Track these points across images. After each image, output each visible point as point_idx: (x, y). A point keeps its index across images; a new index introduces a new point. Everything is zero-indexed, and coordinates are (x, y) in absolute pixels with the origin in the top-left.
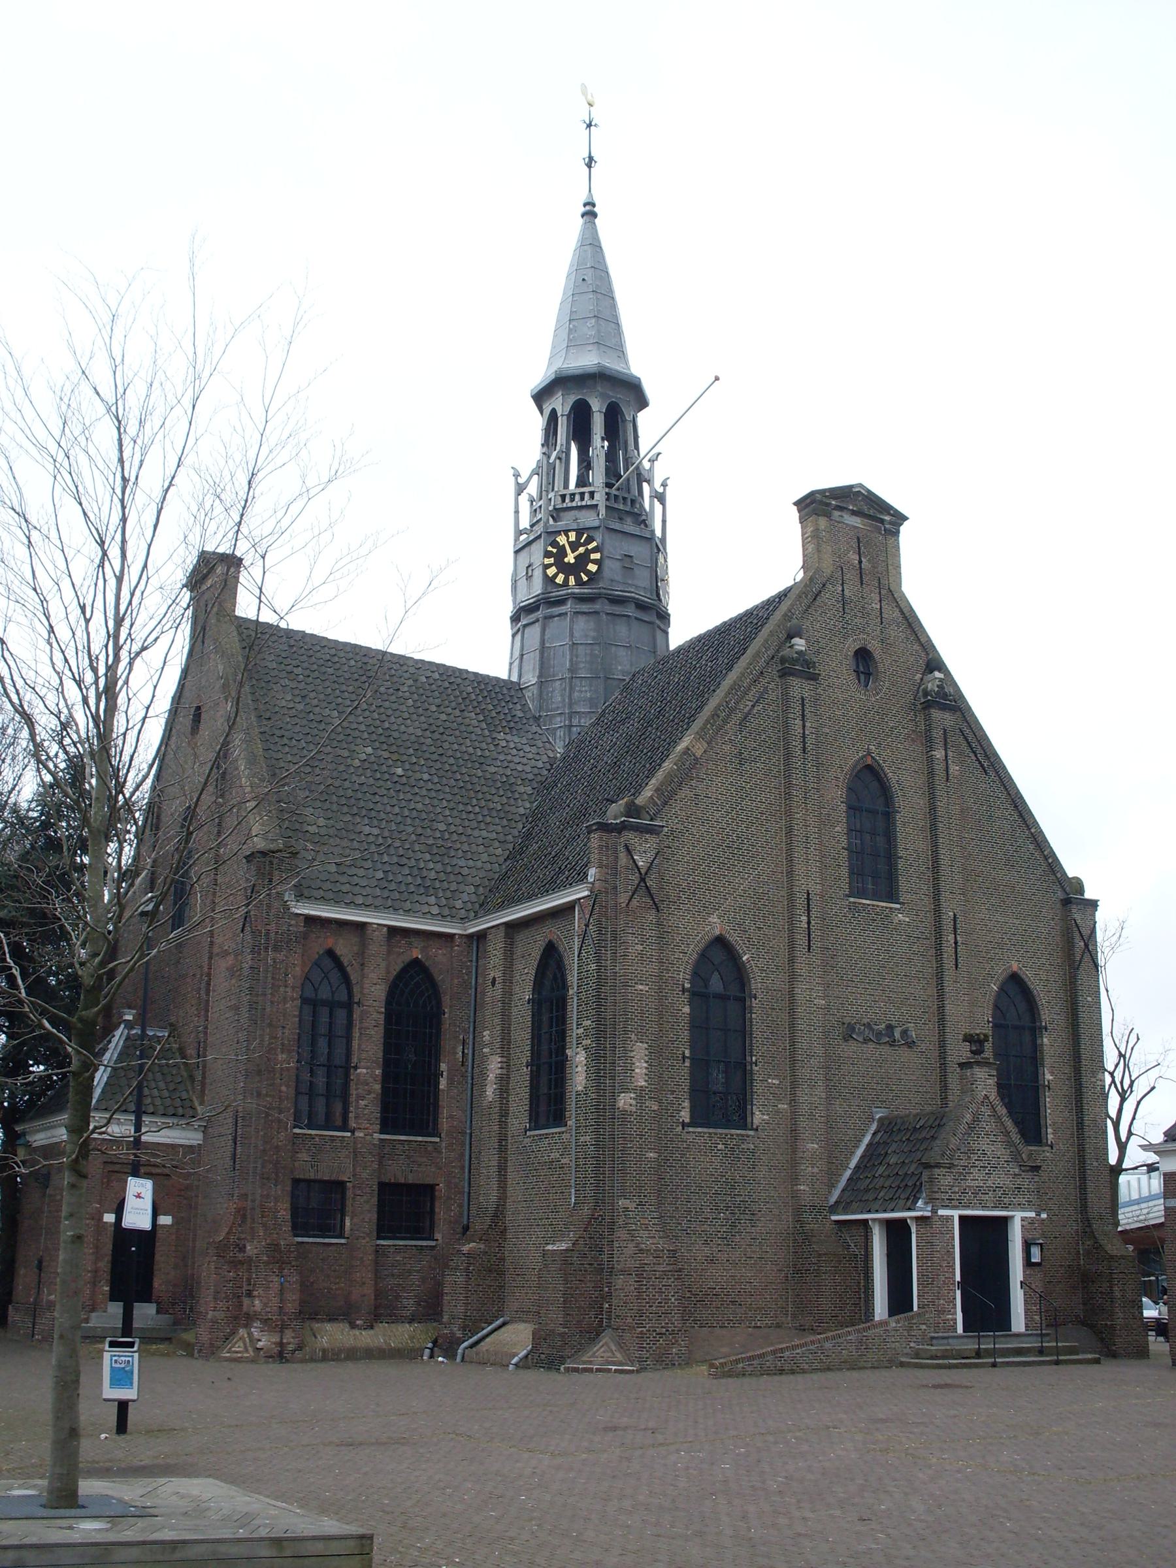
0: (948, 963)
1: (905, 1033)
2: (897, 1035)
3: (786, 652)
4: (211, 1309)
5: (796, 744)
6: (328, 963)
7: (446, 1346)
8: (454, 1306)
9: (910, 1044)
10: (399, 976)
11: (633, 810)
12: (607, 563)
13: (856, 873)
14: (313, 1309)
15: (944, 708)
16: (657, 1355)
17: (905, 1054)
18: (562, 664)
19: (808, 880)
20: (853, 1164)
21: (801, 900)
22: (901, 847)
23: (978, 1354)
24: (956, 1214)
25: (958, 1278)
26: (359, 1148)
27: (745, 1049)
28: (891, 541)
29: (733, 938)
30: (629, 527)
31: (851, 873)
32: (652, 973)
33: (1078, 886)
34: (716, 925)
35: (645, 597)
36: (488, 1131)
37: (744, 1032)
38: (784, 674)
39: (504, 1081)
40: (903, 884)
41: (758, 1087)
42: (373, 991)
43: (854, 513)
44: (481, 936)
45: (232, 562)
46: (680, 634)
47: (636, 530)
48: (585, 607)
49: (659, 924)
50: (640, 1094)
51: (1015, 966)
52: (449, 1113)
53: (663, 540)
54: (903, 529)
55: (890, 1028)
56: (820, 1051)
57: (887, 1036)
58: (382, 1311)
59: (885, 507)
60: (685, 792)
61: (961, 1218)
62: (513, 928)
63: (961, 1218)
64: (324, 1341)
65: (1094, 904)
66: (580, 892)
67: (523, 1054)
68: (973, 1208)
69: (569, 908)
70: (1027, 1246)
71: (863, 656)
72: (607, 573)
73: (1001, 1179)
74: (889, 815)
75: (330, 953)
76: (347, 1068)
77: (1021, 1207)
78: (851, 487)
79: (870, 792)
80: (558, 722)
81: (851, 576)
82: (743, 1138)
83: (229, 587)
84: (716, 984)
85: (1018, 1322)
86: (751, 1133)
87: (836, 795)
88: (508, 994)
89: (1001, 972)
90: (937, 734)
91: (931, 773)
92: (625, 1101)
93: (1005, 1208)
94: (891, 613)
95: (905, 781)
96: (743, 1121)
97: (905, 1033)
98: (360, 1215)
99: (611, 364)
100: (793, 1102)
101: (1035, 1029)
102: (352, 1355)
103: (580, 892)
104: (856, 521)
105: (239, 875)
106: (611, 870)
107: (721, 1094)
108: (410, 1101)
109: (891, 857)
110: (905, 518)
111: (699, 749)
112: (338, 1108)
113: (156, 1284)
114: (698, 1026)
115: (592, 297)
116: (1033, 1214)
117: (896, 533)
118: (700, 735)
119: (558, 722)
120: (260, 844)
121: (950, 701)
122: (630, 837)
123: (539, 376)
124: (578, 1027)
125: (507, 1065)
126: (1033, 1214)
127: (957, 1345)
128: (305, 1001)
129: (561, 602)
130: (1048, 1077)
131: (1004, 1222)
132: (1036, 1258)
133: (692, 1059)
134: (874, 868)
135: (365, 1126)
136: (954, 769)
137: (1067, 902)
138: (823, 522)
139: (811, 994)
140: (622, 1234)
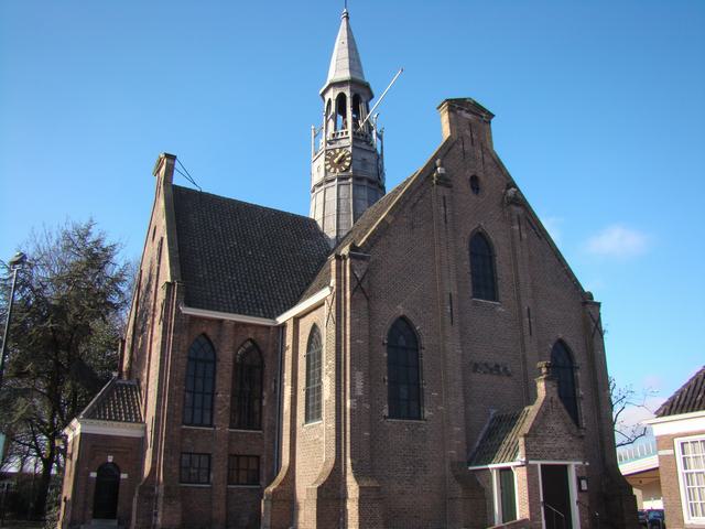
1: (505, 369)
2: (501, 369)
6: (203, 340)
9: (509, 375)
13: (476, 286)
15: (517, 205)
17: (506, 380)
20: (480, 438)
22: (499, 272)
24: (539, 463)
25: (542, 500)
28: (486, 126)
29: (411, 317)
31: (474, 287)
33: (590, 296)
34: (401, 310)
35: (373, 178)
37: (418, 367)
41: (427, 397)
42: (227, 354)
43: (467, 112)
47: (366, 147)
49: (369, 308)
51: (561, 336)
53: (382, 155)
54: (492, 120)
56: (460, 377)
57: (496, 369)
59: (484, 110)
61: (542, 465)
63: (542, 465)
65: (598, 304)
68: (549, 460)
70: (579, 480)
71: (474, 181)
73: (562, 443)
75: (204, 335)
76: (213, 394)
77: (575, 459)
78: (465, 99)
79: (481, 248)
82: (419, 425)
84: (402, 341)
86: (423, 422)
89: (554, 339)
91: (513, 237)
93: (566, 460)
95: (498, 239)
101: (572, 368)
104: (469, 116)
110: (493, 116)
112: (207, 415)
113: (119, 508)
114: (392, 363)
116: (581, 463)
117: (490, 122)
121: (519, 201)
126: (581, 463)
128: (190, 358)
130: (581, 393)
131: (566, 467)
132: (584, 487)
133: (389, 381)
134: (484, 282)
135: (222, 427)
136: (524, 235)
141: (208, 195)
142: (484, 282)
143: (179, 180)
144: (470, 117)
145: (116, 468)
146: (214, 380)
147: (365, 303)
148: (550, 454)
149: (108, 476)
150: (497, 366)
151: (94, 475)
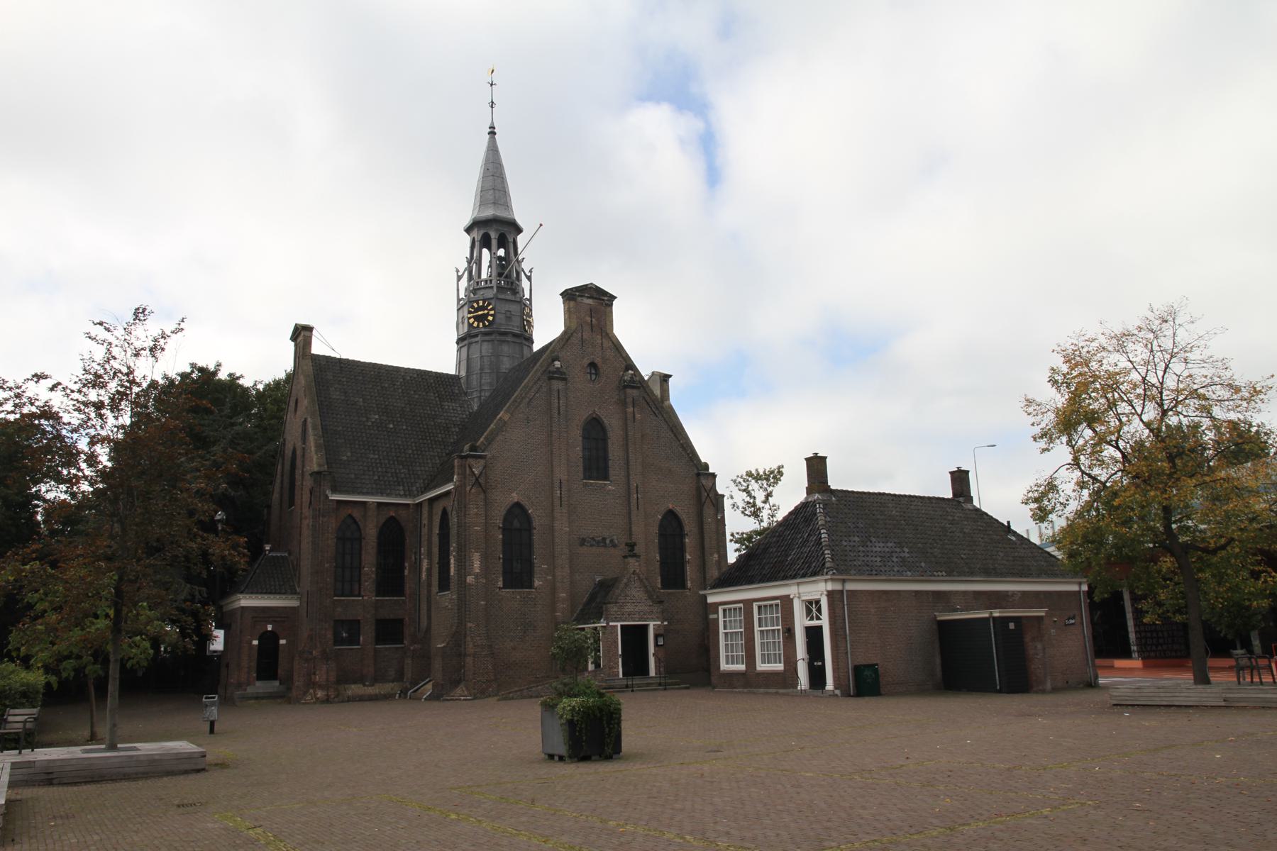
0: (634, 507)
1: (612, 541)
3: (551, 369)
4: (299, 682)
5: (555, 412)
7: (403, 693)
8: (408, 674)
9: (614, 546)
10: (384, 524)
11: (473, 448)
12: (499, 316)
14: (345, 678)
16: (480, 693)
18: (477, 365)
19: (561, 473)
21: (557, 484)
23: (627, 686)
24: (619, 624)
26: (365, 603)
27: (531, 553)
29: (525, 502)
30: (509, 296)
32: (481, 523)
33: (706, 466)
34: (515, 497)
35: (517, 331)
36: (424, 592)
37: (530, 545)
38: (550, 378)
39: (429, 571)
40: (611, 472)
41: (536, 570)
42: (371, 532)
44: (421, 503)
45: (309, 329)
46: (537, 347)
47: (512, 298)
48: (487, 338)
50: (477, 576)
52: (409, 586)
53: (530, 300)
54: (615, 302)
55: (604, 539)
57: (602, 542)
58: (378, 678)
59: (605, 293)
60: (500, 438)
61: (820, 627)
62: (431, 500)
63: (820, 627)
64: (350, 693)
65: (714, 476)
66: (450, 487)
67: (436, 559)
69: (447, 493)
70: (656, 637)
72: (497, 321)
74: (605, 440)
75: (350, 516)
76: (360, 568)
79: (595, 431)
80: (475, 395)
81: (587, 328)
82: (529, 593)
83: (308, 343)
84: (516, 524)
85: (652, 672)
87: (576, 434)
88: (430, 530)
89: (663, 510)
90: (629, 400)
92: (470, 579)
94: (606, 343)
95: (613, 423)
96: (531, 586)
97: (612, 541)
98: (367, 634)
99: (501, 213)
100: (554, 576)
101: (682, 535)
102: (361, 699)
103: (450, 487)
104: (590, 301)
105: (309, 483)
106: (463, 475)
107: (518, 571)
108: (391, 581)
109: (606, 459)
111: (506, 417)
112: (356, 587)
115: (494, 180)
118: (507, 411)
119: (475, 395)
120: (316, 468)
122: (471, 461)
123: (467, 221)
124: (453, 546)
125: (430, 563)
127: (617, 683)
129: (476, 336)
130: (688, 557)
131: (646, 627)
132: (661, 643)
134: (596, 465)
135: (368, 595)
136: (638, 416)
137: (698, 475)
138: (572, 303)
139: (562, 526)
140: (469, 639)
141: (347, 361)
142: (596, 465)
143: (318, 348)
144: (589, 304)
145: (274, 636)
146: (360, 554)
147: (482, 496)
148: (630, 616)
149: (269, 640)
150: (604, 539)
151: (255, 642)
